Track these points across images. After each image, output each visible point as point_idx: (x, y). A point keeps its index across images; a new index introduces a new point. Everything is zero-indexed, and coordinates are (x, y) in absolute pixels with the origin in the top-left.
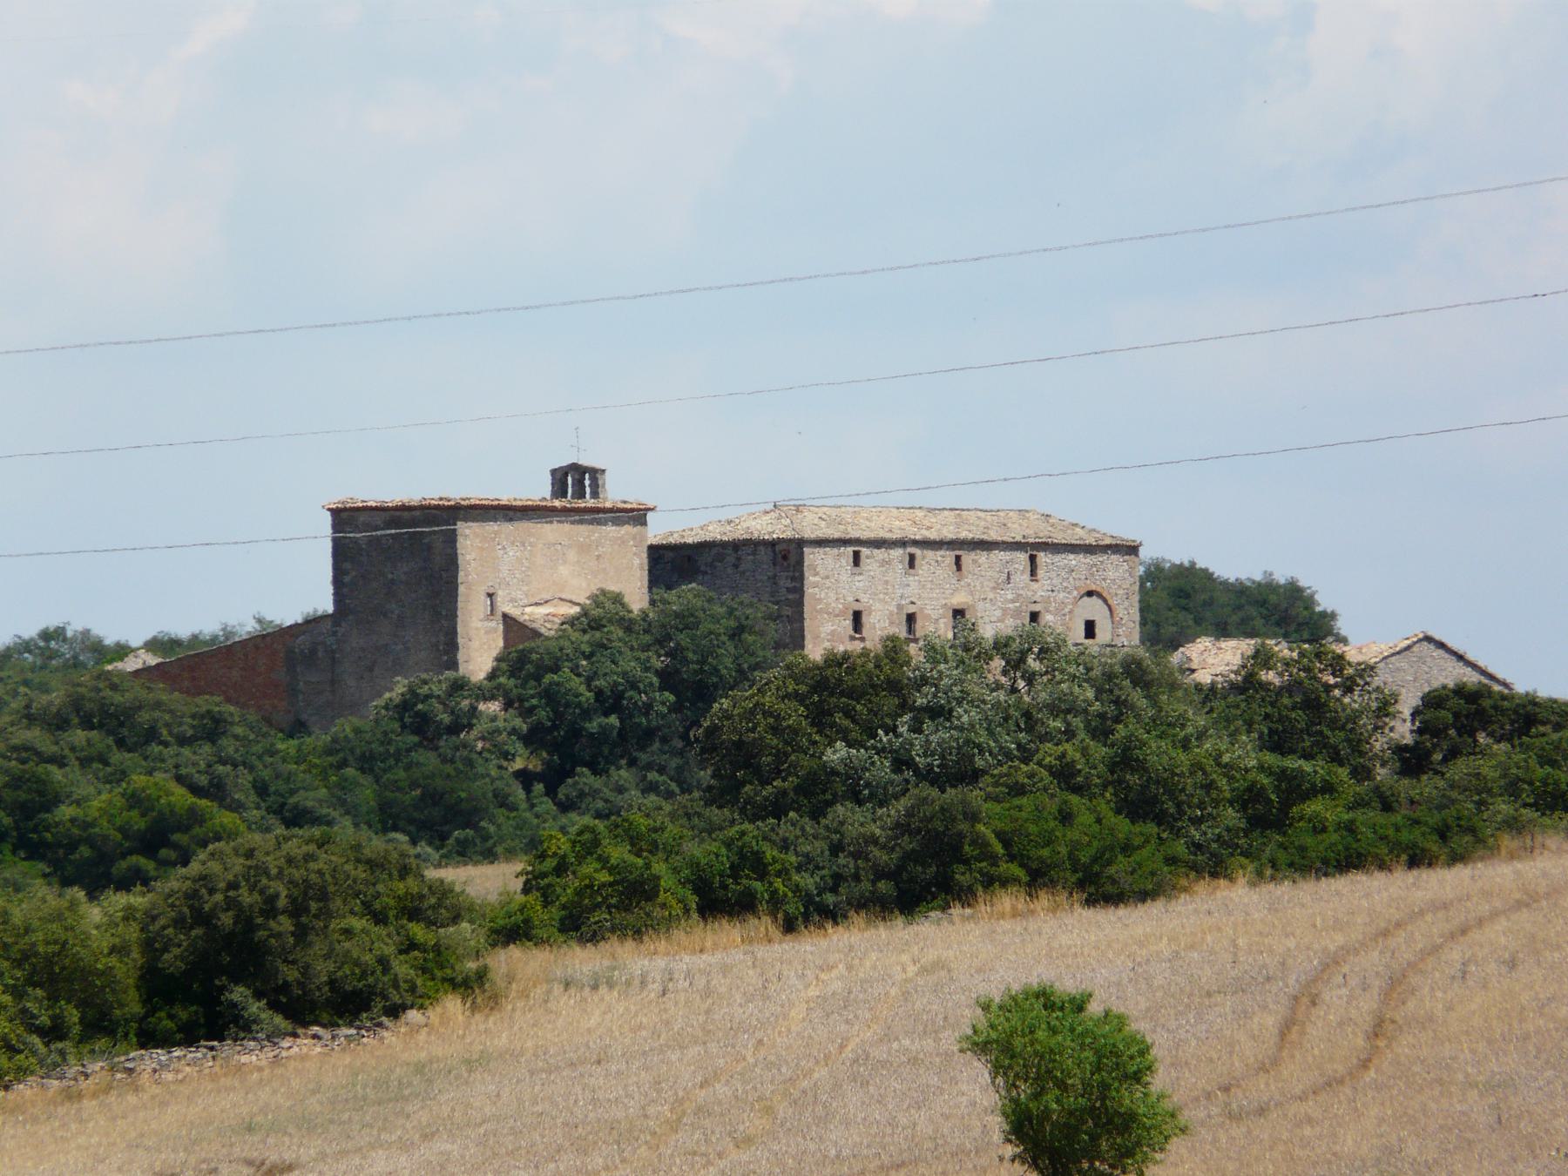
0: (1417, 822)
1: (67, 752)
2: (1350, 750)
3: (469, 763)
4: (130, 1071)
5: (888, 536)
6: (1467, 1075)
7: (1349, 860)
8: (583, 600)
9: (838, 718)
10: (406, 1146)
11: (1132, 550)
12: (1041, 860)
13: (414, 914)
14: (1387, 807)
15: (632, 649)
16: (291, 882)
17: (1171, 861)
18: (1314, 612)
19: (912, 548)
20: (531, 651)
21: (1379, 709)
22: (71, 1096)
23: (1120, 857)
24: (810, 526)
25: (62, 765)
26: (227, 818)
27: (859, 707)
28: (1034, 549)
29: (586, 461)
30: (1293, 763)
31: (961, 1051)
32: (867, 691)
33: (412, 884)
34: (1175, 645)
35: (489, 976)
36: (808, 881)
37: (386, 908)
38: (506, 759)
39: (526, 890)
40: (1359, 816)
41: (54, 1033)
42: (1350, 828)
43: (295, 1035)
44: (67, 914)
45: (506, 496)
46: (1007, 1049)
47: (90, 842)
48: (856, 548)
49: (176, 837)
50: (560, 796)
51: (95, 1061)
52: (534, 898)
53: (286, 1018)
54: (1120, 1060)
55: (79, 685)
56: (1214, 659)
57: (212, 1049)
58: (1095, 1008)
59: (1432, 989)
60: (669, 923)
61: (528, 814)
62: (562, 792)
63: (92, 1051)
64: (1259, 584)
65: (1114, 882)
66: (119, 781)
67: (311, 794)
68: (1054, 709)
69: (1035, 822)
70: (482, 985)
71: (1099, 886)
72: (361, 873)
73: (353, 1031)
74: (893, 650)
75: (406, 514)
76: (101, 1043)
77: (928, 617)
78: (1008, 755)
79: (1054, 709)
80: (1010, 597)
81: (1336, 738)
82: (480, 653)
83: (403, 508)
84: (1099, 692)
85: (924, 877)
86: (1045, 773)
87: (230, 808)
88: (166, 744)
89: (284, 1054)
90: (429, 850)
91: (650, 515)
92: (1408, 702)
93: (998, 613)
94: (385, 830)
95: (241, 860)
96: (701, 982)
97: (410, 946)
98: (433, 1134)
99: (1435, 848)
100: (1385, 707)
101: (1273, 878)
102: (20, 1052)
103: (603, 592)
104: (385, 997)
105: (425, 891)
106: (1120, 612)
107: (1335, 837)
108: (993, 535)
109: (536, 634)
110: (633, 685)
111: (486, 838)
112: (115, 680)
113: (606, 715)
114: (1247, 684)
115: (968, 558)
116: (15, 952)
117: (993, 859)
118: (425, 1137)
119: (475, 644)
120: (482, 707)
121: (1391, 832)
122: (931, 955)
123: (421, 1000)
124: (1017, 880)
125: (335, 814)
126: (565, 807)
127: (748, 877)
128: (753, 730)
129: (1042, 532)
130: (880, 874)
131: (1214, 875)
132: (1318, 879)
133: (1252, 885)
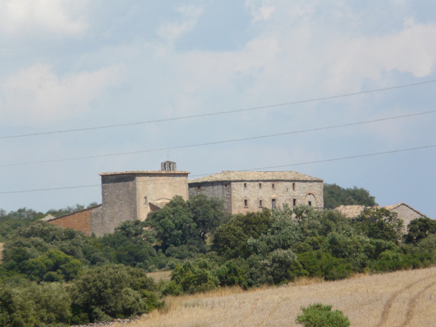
1: (30, 243)
9: (252, 231)
11: (322, 181)
15: (185, 212)
16: (111, 279)
17: (348, 268)
19: (260, 182)
20: (157, 213)
23: (334, 267)
24: (233, 177)
26: (76, 261)
27: (257, 228)
28: (294, 181)
31: (297, 323)
32: (253, 223)
33: (143, 278)
38: (151, 243)
39: (172, 279)
43: (113, 321)
45: (149, 171)
47: (37, 268)
48: (244, 182)
50: (166, 253)
56: (352, 211)
57: (91, 325)
58: (333, 310)
59: (422, 303)
60: (212, 288)
61: (158, 258)
62: (167, 251)
65: (332, 274)
67: (98, 253)
68: (309, 228)
69: (311, 258)
70: (163, 306)
71: (328, 276)
73: (128, 320)
77: (265, 201)
78: (297, 240)
80: (288, 195)
81: (386, 233)
82: (143, 214)
83: (123, 174)
84: (321, 222)
85: (281, 275)
86: (307, 244)
87: (77, 258)
92: (407, 222)
95: (97, 274)
97: (144, 296)
101: (376, 273)
103: (177, 196)
104: (137, 310)
106: (318, 199)
108: (282, 178)
109: (158, 208)
110: (185, 221)
111: (146, 264)
113: (179, 230)
114: (361, 219)
115: (277, 185)
117: (299, 269)
119: (141, 211)
122: (285, 296)
124: (306, 275)
125: (105, 259)
126: (168, 255)
127: (233, 276)
130: (268, 273)
131: (359, 272)
133: (371, 275)
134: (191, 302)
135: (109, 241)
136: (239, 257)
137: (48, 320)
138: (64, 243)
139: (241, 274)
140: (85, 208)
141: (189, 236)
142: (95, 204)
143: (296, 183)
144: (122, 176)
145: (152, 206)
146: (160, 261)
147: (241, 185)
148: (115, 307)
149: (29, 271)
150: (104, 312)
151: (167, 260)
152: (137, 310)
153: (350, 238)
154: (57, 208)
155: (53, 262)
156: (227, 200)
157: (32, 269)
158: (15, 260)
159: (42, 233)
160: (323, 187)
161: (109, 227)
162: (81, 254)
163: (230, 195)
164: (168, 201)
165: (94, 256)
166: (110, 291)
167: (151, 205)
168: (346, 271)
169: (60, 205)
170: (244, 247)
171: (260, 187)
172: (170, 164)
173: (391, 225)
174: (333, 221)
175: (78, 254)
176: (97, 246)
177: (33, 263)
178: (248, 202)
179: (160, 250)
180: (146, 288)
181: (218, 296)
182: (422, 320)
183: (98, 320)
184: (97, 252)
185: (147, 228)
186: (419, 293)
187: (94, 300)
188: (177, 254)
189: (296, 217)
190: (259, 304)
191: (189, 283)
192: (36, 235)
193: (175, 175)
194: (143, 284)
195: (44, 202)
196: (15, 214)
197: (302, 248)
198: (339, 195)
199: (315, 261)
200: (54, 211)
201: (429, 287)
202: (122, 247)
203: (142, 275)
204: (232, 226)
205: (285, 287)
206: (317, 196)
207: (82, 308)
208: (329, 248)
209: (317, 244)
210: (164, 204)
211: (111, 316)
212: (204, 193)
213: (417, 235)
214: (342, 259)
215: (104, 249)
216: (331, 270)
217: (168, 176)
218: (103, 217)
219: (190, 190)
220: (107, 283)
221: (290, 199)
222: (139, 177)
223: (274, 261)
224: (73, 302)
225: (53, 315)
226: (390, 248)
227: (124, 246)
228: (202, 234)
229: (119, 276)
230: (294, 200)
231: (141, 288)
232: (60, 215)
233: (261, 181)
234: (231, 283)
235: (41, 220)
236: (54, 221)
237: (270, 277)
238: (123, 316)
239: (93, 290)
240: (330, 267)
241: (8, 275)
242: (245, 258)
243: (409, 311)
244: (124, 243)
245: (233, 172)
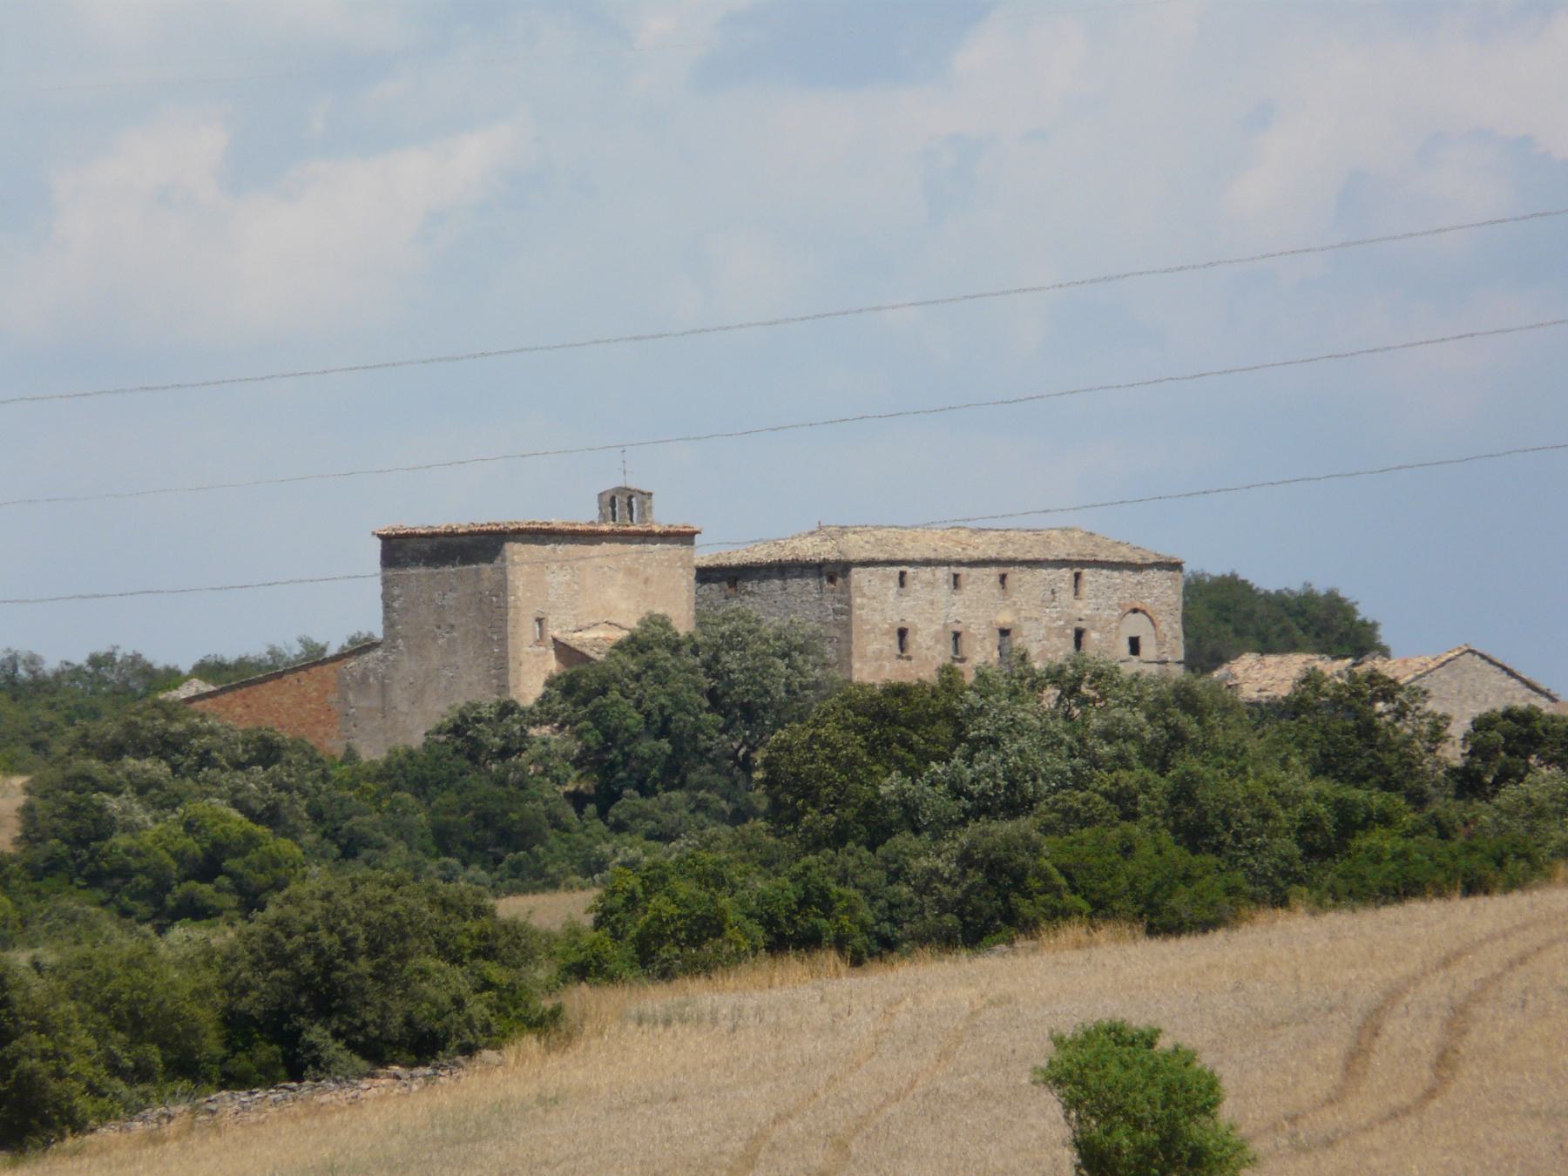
0: (1474, 849)
3: (522, 786)
4: (212, 1112)
5: (932, 555)
7: (1404, 888)
11: (1176, 566)
12: (1104, 892)
13: (489, 953)
14: (1444, 833)
17: (1232, 891)
18: (1353, 622)
19: (957, 568)
21: (1432, 734)
22: (155, 1139)
23: (1182, 887)
24: (856, 547)
26: (285, 846)
27: (915, 737)
28: (1077, 565)
29: (633, 483)
31: (1034, 1083)
32: (907, 722)
34: (1218, 660)
37: (460, 948)
39: (598, 924)
41: (141, 1073)
42: (1403, 854)
43: (372, 1076)
45: (557, 521)
46: (1082, 1083)
47: (143, 870)
48: (901, 568)
49: (231, 863)
50: (611, 819)
51: (177, 1103)
54: (1190, 1093)
56: (1264, 676)
57: (293, 1090)
58: (1164, 1044)
60: (737, 958)
65: (1174, 912)
66: (173, 807)
67: (367, 819)
68: (1108, 736)
69: (1099, 856)
71: (1160, 920)
73: (428, 1071)
76: (183, 1085)
79: (1108, 736)
81: (1389, 759)
82: (531, 680)
84: (1151, 718)
85: (990, 910)
86: (1098, 797)
87: (285, 835)
88: (223, 769)
89: (362, 1095)
90: (483, 873)
92: (1458, 729)
93: (1043, 631)
97: (487, 985)
100: (1437, 734)
101: (1334, 906)
102: (103, 1095)
106: (1163, 627)
107: (1392, 866)
109: (585, 659)
110: (680, 706)
111: (537, 859)
113: (657, 738)
114: (1293, 708)
115: (1014, 574)
117: (1057, 889)
120: (533, 731)
121: (1447, 860)
123: (496, 1039)
124: (1080, 913)
125: (387, 839)
126: (619, 827)
127: (817, 915)
129: (1088, 551)
130: (943, 906)
131: (1274, 905)
133: (1313, 914)
135: (409, 775)
136: (851, 845)
138: (239, 778)
140: (332, 650)
144: (447, 540)
145: (564, 651)
147: (888, 577)
149: (117, 881)
150: (340, 1045)
152: (458, 1036)
153: (1278, 776)
155: (203, 849)
157: (125, 873)
159: (166, 743)
162: (305, 822)
163: (849, 612)
164: (621, 635)
166: (364, 965)
172: (630, 498)
175: (291, 822)
176: (364, 791)
178: (909, 637)
179: (591, 809)
180: (496, 958)
182: (1488, 1082)
183: (322, 1070)
184: (363, 813)
186: (1485, 984)
188: (650, 825)
190: (903, 1018)
191: (661, 938)
192: (141, 752)
193: (647, 537)
194: (483, 944)
198: (1249, 615)
199: (1113, 865)
202: (450, 797)
203: (479, 912)
205: (1003, 954)
207: (261, 1029)
208: (1165, 817)
210: (607, 646)
211: (364, 1056)
214: (1211, 859)
216: (1169, 896)
217: (623, 542)
218: (384, 689)
219: (701, 592)
220: (355, 939)
221: (1062, 629)
224: (230, 1006)
226: (1386, 820)
227: (459, 793)
230: (1079, 634)
231: (476, 954)
232: (229, 677)
233: (959, 563)
234: (809, 942)
235: (162, 696)
236: (209, 701)
237: (950, 920)
241: (39, 896)
242: (872, 847)
243: (1446, 1050)
244: (459, 784)
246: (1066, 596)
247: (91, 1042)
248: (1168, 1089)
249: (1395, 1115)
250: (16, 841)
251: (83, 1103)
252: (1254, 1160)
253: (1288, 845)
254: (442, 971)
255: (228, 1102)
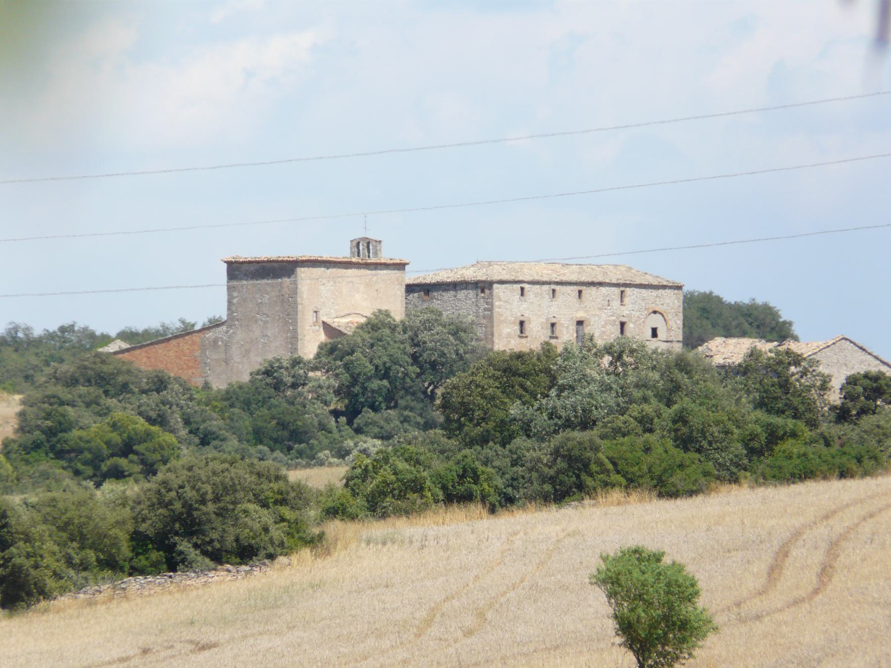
0: (844, 453)
2: (803, 411)
4: (124, 589)
6: (874, 598)
8: (369, 314)
10: (278, 634)
11: (679, 288)
12: (633, 473)
13: (283, 502)
17: (706, 474)
18: (778, 322)
19: (555, 285)
20: (339, 343)
21: (822, 385)
22: (90, 603)
23: (678, 471)
24: (496, 273)
25: (74, 406)
26: (169, 438)
27: (528, 383)
30: (778, 420)
31: (591, 584)
32: (523, 374)
33: (281, 483)
35: (325, 537)
36: (499, 482)
39: (347, 485)
40: (810, 450)
41: (84, 566)
43: (215, 569)
44: (89, 501)
45: (326, 256)
47: (89, 450)
48: (521, 285)
50: (355, 425)
52: (348, 493)
53: (212, 560)
54: (681, 589)
55: (83, 360)
56: (727, 350)
57: (170, 577)
58: (667, 560)
62: (357, 421)
63: (103, 578)
64: (748, 305)
65: (674, 485)
69: (631, 452)
71: (666, 490)
72: (254, 478)
73: (247, 568)
74: (548, 350)
75: (270, 264)
76: (108, 573)
77: (562, 325)
81: (796, 401)
82: (310, 344)
84: (662, 375)
85: (568, 482)
89: (210, 580)
90: (281, 455)
91: (407, 267)
92: (837, 382)
94: (256, 445)
95: (185, 472)
96: (443, 542)
97: (283, 520)
98: (294, 627)
99: (854, 468)
100: (824, 387)
101: (764, 484)
103: (380, 311)
105: (289, 489)
107: (798, 461)
108: (600, 279)
111: (312, 448)
112: (103, 357)
114: (743, 370)
115: (586, 291)
116: (60, 523)
118: (289, 628)
119: (307, 338)
121: (829, 458)
122: (572, 528)
123: (285, 549)
126: (358, 431)
127: (470, 483)
128: (470, 396)
130: (544, 479)
131: (730, 482)
132: (789, 485)
133: (752, 488)
134: (378, 534)
136: (491, 444)
137: (81, 564)
138: (144, 398)
139: (486, 480)
140: (197, 328)
141: (402, 393)
142: (217, 320)
143: (628, 291)
146: (342, 442)
148: (222, 540)
150: (198, 552)
151: (356, 440)
154: (139, 326)
156: (484, 321)
158: (43, 432)
160: (682, 298)
161: (241, 369)
164: (363, 320)
165: (206, 428)
166: (211, 507)
167: (327, 327)
168: (703, 480)
169: (144, 321)
170: (502, 424)
171: (554, 297)
172: (368, 243)
173: (807, 384)
174: (687, 373)
177: (80, 438)
180: (287, 504)
181: (437, 524)
182: (850, 585)
183: (187, 566)
185: (318, 373)
186: (849, 530)
187: (177, 525)
188: (376, 430)
189: (611, 363)
195: (109, 316)
196: (51, 336)
197: (620, 428)
198: (720, 315)
200: (132, 332)
201: (871, 516)
202: (265, 411)
203: (278, 478)
204: (478, 379)
206: (669, 317)
207: (152, 542)
209: (652, 420)
212: (436, 304)
213: (859, 405)
215: (226, 415)
218: (227, 346)
220: (206, 493)
221: (614, 321)
222: (306, 269)
223: (556, 453)
225: (91, 555)
228: (431, 388)
229: (232, 479)
231: (276, 502)
232: (137, 340)
233: (557, 283)
234: (466, 498)
235: (100, 350)
237: (547, 487)
238: (238, 560)
239: (178, 506)
240: (670, 470)
241: (27, 462)
242: (504, 446)
245: (496, 263)
246: (616, 303)
247: (56, 548)
248: (669, 585)
249: (797, 602)
250: (16, 431)
251: (50, 583)
252: (715, 629)
253: (738, 448)
254: (256, 512)
255: (134, 583)
